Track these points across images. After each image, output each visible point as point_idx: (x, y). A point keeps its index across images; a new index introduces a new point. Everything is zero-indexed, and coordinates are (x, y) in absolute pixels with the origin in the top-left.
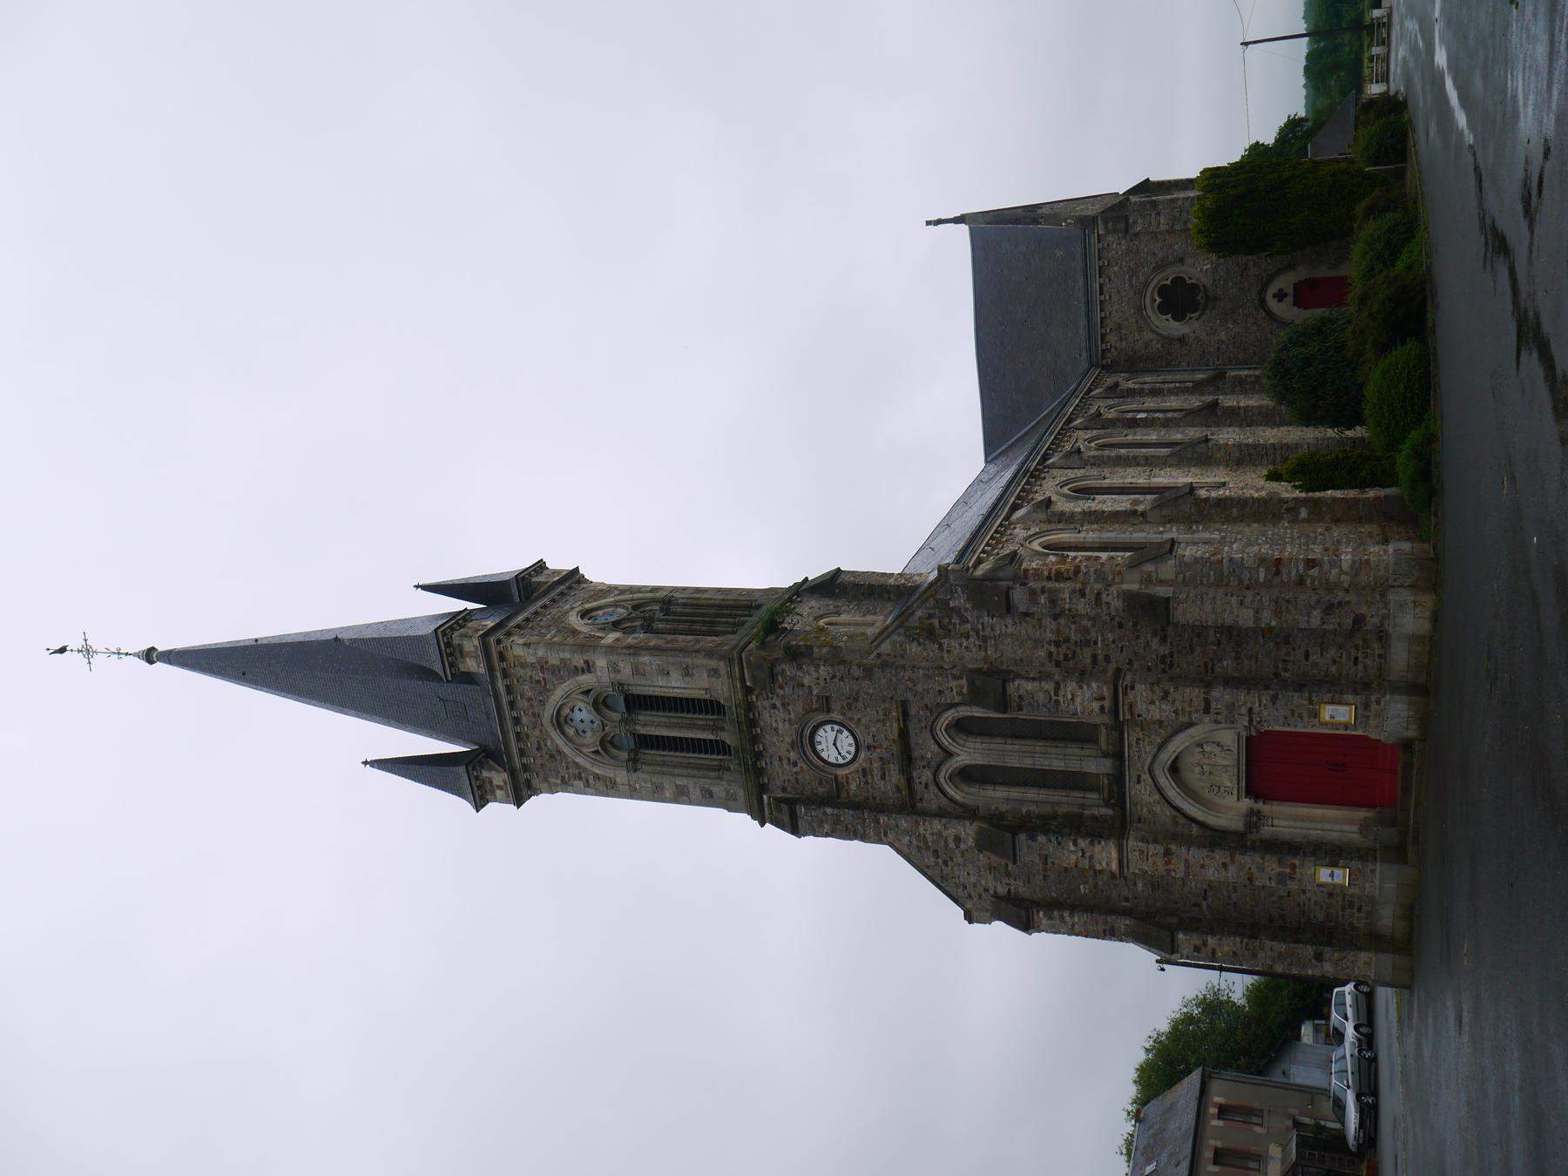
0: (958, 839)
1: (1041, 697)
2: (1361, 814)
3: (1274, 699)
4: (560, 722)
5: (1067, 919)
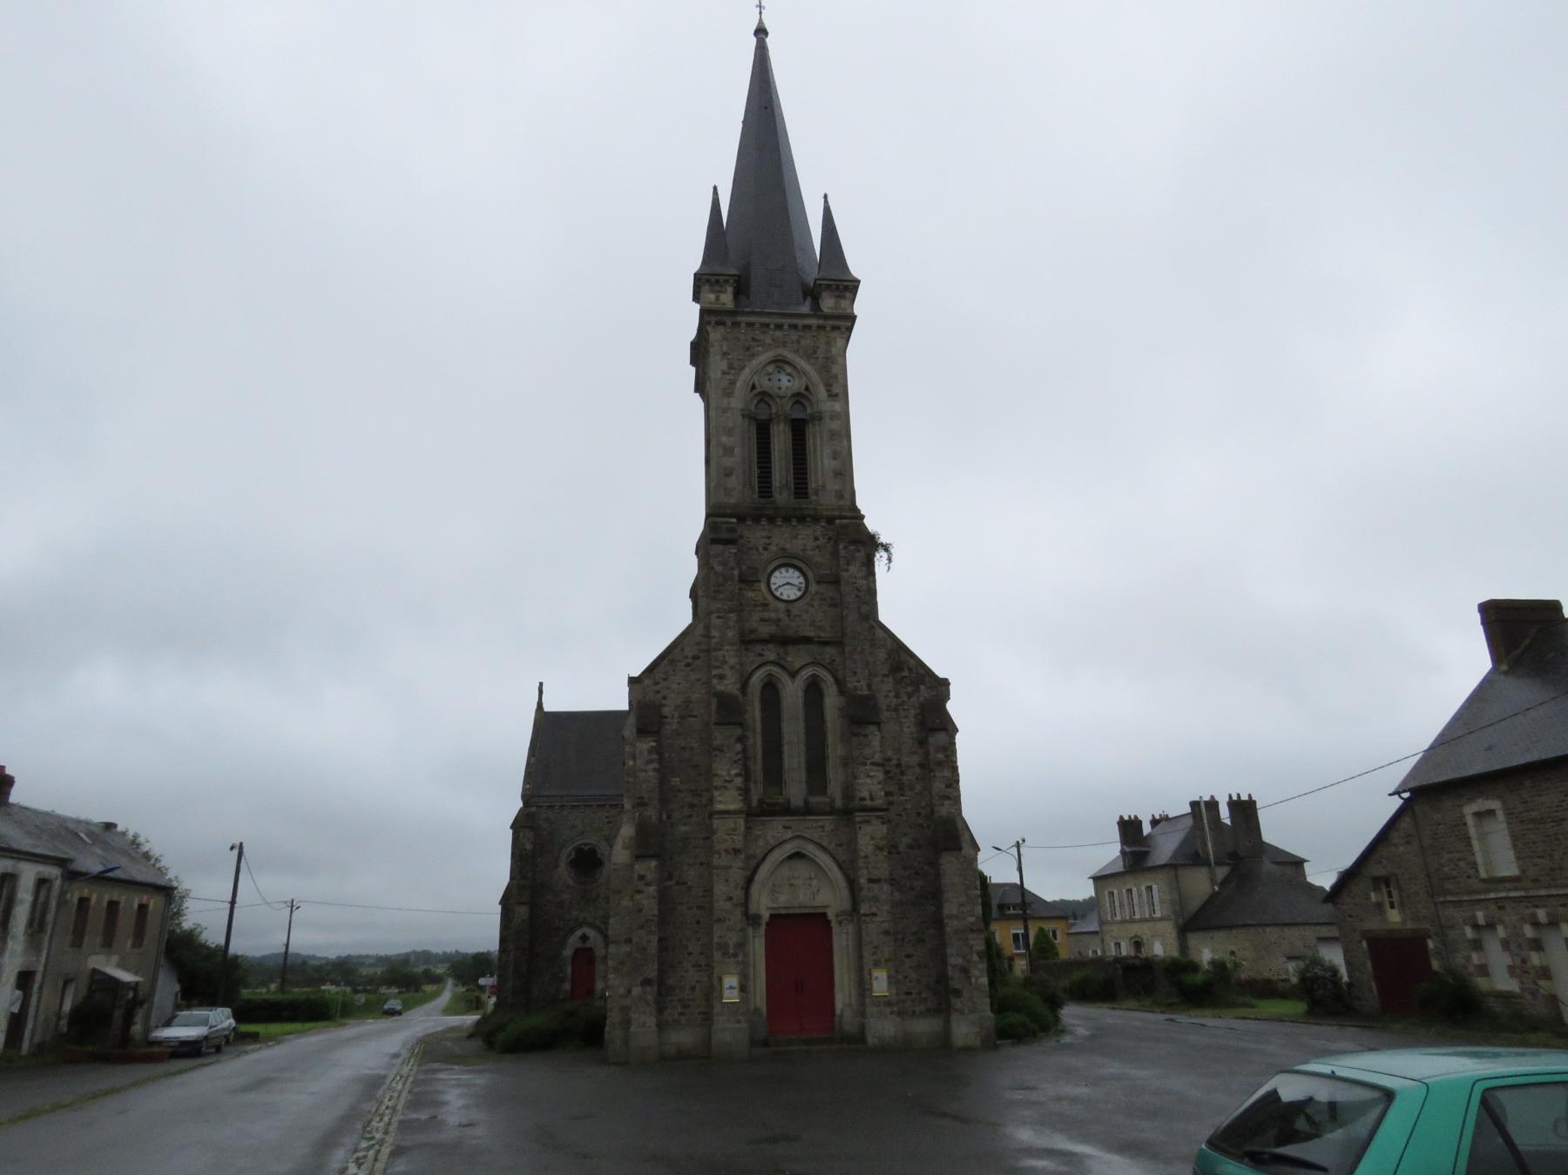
0: (721, 677)
1: (867, 751)
2: (764, 1009)
3: (886, 933)
4: (780, 362)
5: (652, 766)
